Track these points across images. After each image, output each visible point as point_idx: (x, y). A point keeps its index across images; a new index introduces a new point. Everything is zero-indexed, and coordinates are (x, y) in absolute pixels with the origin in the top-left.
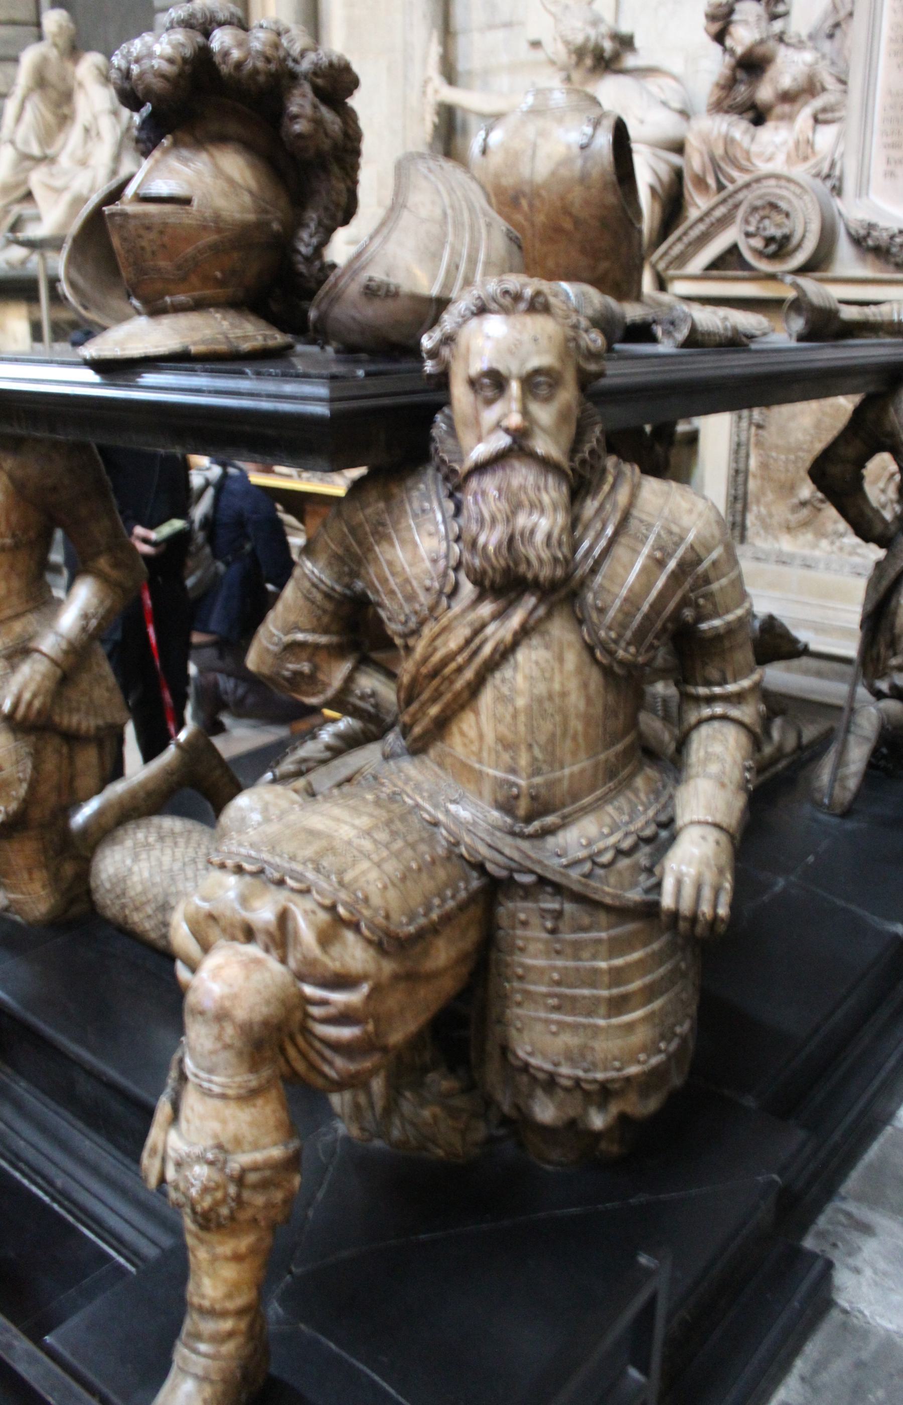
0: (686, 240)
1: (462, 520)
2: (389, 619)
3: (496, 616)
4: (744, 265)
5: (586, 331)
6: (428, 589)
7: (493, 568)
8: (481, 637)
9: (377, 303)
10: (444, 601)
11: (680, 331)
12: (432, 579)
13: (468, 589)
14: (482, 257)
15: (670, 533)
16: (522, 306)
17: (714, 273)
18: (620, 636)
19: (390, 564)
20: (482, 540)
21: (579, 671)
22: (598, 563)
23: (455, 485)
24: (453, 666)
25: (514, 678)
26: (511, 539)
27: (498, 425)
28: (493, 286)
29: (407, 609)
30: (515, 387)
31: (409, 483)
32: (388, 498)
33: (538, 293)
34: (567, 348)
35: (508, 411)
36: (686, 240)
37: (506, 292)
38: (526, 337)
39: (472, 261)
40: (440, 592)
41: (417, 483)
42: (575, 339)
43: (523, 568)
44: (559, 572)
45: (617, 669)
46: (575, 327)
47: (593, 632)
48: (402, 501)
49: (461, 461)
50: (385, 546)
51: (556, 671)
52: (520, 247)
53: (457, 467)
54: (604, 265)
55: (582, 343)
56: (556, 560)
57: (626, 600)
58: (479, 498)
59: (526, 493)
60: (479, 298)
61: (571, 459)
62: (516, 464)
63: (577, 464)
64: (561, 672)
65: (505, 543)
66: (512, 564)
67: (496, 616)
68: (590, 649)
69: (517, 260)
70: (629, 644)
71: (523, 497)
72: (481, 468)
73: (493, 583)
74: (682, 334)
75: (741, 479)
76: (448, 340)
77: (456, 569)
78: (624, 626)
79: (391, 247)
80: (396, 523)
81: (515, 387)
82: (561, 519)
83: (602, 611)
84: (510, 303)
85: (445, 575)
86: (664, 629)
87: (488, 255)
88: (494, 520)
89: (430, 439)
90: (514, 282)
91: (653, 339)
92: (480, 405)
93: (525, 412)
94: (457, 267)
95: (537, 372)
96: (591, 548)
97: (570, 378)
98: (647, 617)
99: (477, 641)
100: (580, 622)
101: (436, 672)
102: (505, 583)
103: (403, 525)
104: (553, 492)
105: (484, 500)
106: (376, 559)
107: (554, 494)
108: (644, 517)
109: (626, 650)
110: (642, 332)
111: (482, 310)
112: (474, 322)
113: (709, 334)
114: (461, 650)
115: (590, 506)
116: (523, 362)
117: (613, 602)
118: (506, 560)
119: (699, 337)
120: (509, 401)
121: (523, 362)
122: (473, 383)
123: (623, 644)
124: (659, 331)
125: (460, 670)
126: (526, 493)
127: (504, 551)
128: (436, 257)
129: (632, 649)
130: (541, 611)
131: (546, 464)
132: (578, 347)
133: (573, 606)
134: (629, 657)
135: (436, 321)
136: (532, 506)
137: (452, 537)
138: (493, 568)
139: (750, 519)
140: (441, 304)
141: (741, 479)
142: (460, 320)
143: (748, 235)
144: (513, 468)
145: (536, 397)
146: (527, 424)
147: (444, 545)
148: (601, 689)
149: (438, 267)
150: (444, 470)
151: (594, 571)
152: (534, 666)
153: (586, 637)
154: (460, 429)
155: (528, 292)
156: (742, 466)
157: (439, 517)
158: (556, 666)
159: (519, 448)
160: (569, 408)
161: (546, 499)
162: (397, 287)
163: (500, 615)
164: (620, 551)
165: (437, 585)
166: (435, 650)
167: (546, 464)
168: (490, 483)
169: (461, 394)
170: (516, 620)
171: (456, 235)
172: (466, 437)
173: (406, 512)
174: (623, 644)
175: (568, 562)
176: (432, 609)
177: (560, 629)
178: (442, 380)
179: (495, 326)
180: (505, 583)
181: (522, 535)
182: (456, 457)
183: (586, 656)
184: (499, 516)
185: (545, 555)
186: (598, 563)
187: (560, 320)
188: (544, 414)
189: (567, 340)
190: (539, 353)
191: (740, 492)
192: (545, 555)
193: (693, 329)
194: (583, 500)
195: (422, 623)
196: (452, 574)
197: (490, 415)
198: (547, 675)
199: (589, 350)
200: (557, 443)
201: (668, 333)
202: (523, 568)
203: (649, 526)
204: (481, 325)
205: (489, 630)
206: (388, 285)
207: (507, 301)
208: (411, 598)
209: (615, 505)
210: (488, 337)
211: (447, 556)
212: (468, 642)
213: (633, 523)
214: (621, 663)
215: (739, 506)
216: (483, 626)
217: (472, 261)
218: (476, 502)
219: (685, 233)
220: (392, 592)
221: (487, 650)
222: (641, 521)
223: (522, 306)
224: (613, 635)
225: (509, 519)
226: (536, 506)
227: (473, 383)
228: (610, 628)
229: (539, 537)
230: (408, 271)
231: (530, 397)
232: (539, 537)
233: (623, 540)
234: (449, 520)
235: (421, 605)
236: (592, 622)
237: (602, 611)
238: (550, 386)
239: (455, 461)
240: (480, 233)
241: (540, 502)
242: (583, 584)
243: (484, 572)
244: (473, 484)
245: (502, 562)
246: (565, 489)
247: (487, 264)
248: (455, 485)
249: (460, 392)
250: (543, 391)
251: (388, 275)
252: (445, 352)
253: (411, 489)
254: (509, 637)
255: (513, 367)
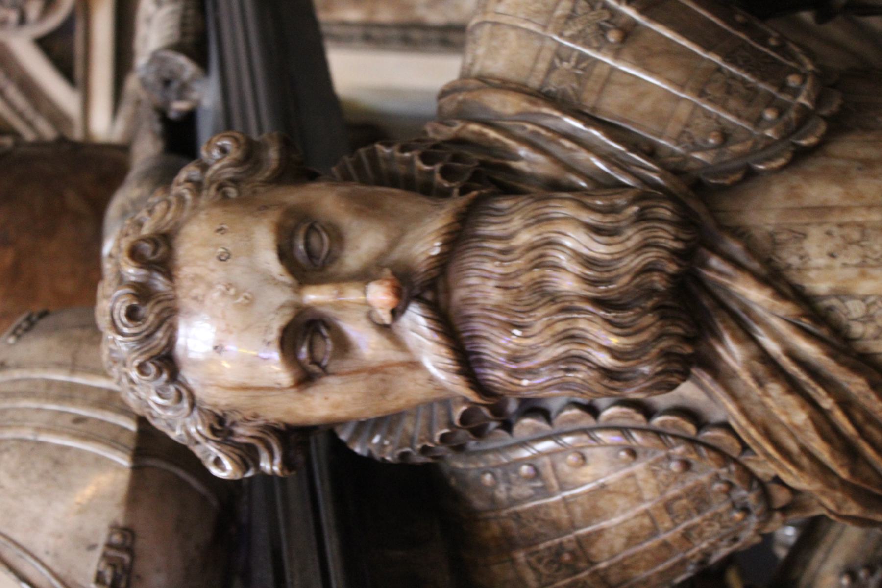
0: (30, 113)
1: (556, 401)
2: (735, 540)
3: (747, 336)
4: (66, 29)
5: (204, 167)
6: (686, 465)
7: (659, 337)
8: (785, 361)
9: (143, 566)
10: (708, 434)
11: (182, 67)
12: (669, 458)
13: (688, 392)
14: (61, 376)
15: (570, 17)
16: (160, 283)
17: (79, 72)
18: (771, 102)
19: (632, 539)
20: (605, 359)
21: (841, 177)
22: (635, 143)
23: (494, 410)
24: (839, 417)
25: (864, 299)
26: (598, 302)
27: (384, 329)
28: (120, 344)
29: (721, 506)
30: (316, 296)
31: (479, 503)
32: (507, 543)
33: (134, 254)
34: (242, 201)
35: (359, 308)
36: (30, 113)
37: (132, 314)
38: (218, 273)
39: (68, 393)
40: (692, 442)
41: (480, 488)
42: (221, 187)
43: (658, 282)
44: (665, 212)
45: (834, 106)
46: (198, 187)
47: (768, 148)
48: (517, 516)
49: (446, 403)
50: (600, 549)
51: (847, 218)
52: (44, 314)
53: (459, 411)
54: (72, 199)
55: (229, 173)
56: (641, 218)
57: (701, 94)
58: (526, 365)
59: (516, 275)
60: (142, 368)
61: (445, 194)
62: (459, 294)
63: (455, 186)
64: (844, 209)
65: (610, 315)
66: (649, 304)
67: (747, 336)
68: (800, 156)
69: (68, 317)
70: (783, 87)
71: (525, 278)
72: (467, 361)
73: (686, 339)
74: (186, 66)
75: (376, 33)
76: (221, 427)
77: (648, 412)
78: (751, 96)
79: (40, 542)
80: (557, 528)
81: (316, 296)
82: (563, 208)
83: (726, 136)
84: (155, 309)
85: (658, 433)
86: (743, 27)
87: (59, 365)
88: (569, 337)
89: (404, 463)
90: (111, 301)
91: (190, 118)
92: (348, 364)
93: (364, 277)
94: (79, 420)
95: (285, 255)
96: (607, 157)
97: (294, 196)
98: (729, 57)
99: (793, 369)
100: (750, 174)
101: (847, 450)
102: (683, 316)
103: (563, 516)
104: (513, 226)
105: (525, 358)
106: (623, 566)
107: (517, 222)
108: (542, 66)
109: (795, 92)
110: (180, 137)
111: (167, 362)
112: (189, 375)
113: (183, 25)
114: (810, 402)
115: (529, 161)
116: (272, 281)
117: (708, 115)
118: (645, 312)
119: (189, 39)
120: (340, 306)
121: (272, 281)
122: (305, 379)
123: (785, 97)
124: (179, 106)
125: (846, 403)
126: (516, 275)
127: (627, 316)
128: (59, 459)
129: (793, 81)
130: (735, 247)
131: (459, 239)
132: (235, 182)
133: (722, 188)
134: (808, 86)
135: (182, 455)
136: (540, 263)
137: (588, 421)
138: (659, 337)
139: (435, 17)
140: (150, 447)
141: (376, 33)
142: (186, 404)
143: (22, 20)
144: (468, 301)
145: (333, 257)
146: (387, 272)
147: (606, 437)
148: (870, 137)
149: (80, 453)
150: (463, 434)
151: (651, 152)
152: (837, 263)
153: (781, 161)
154: (391, 404)
155: (132, 272)
156: (357, 31)
157: (547, 445)
158: (835, 218)
159: (428, 289)
160: (351, 198)
161: (525, 237)
162: (114, 528)
163: (743, 326)
164: (611, 105)
165: (679, 450)
166: (805, 451)
167: (459, 239)
168: (496, 346)
169: (327, 403)
170: (754, 295)
171: (19, 424)
172: (410, 390)
173: (537, 508)
174: (785, 97)
175: (647, 194)
176: (725, 458)
177: (765, 212)
178: (294, 438)
179: (195, 338)
180: (683, 316)
181: (593, 283)
182: (439, 412)
183: (813, 165)
184: (560, 327)
185: (633, 237)
186: (635, 143)
187: (186, 214)
188: (365, 242)
189: (224, 200)
190: (251, 251)
191: (394, 33)
192: (633, 237)
193: (178, 47)
194: (517, 174)
195: (749, 477)
196: (657, 421)
197: (368, 344)
198: (856, 235)
199: (237, 163)
200: (417, 219)
201: (183, 91)
202: (658, 282)
203: (560, 54)
204: (196, 363)
205: (773, 347)
206: (110, 545)
207: (150, 313)
208: (699, 499)
209: (524, 117)
210: (218, 348)
211: (624, 430)
212: (793, 387)
213: (553, 84)
214: (819, 100)
215: (416, 35)
216: (765, 357)
217: (68, 393)
218: (531, 372)
219: (21, 115)
220: (686, 535)
221: (809, 349)
222: (552, 68)
223: (160, 283)
224: (769, 115)
225: (566, 307)
226: (540, 256)
227: (305, 379)
228: (758, 121)
229: (598, 249)
230: (83, 510)
231: (332, 269)
232: (598, 249)
233: (589, 100)
234: (557, 428)
235: (717, 478)
236: (753, 151)
237: (726, 136)
238: (312, 229)
239: (449, 415)
240: (15, 381)
241: (533, 247)
242: (676, 170)
243: (666, 355)
244: (496, 376)
245: (649, 319)
246: (505, 204)
247: (73, 368)
248: (494, 410)
249: (321, 404)
250: (322, 243)
251: (92, 547)
252: (244, 433)
253: (493, 499)
254: (787, 308)
255: (276, 301)
